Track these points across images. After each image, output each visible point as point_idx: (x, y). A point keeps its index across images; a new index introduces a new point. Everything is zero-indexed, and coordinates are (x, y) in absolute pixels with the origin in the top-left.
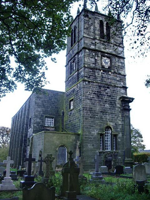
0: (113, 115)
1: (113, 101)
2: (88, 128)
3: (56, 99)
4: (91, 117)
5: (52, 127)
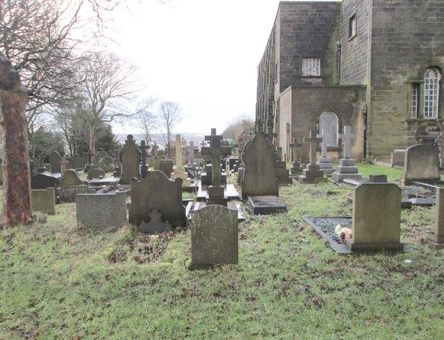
5: (317, 77)
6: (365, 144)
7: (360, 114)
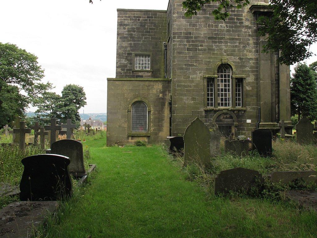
0: (235, 43)
1: (235, 15)
2: (182, 69)
3: (152, 23)
4: (188, 49)
5: (148, 72)
6: (170, 130)
7: (167, 104)
